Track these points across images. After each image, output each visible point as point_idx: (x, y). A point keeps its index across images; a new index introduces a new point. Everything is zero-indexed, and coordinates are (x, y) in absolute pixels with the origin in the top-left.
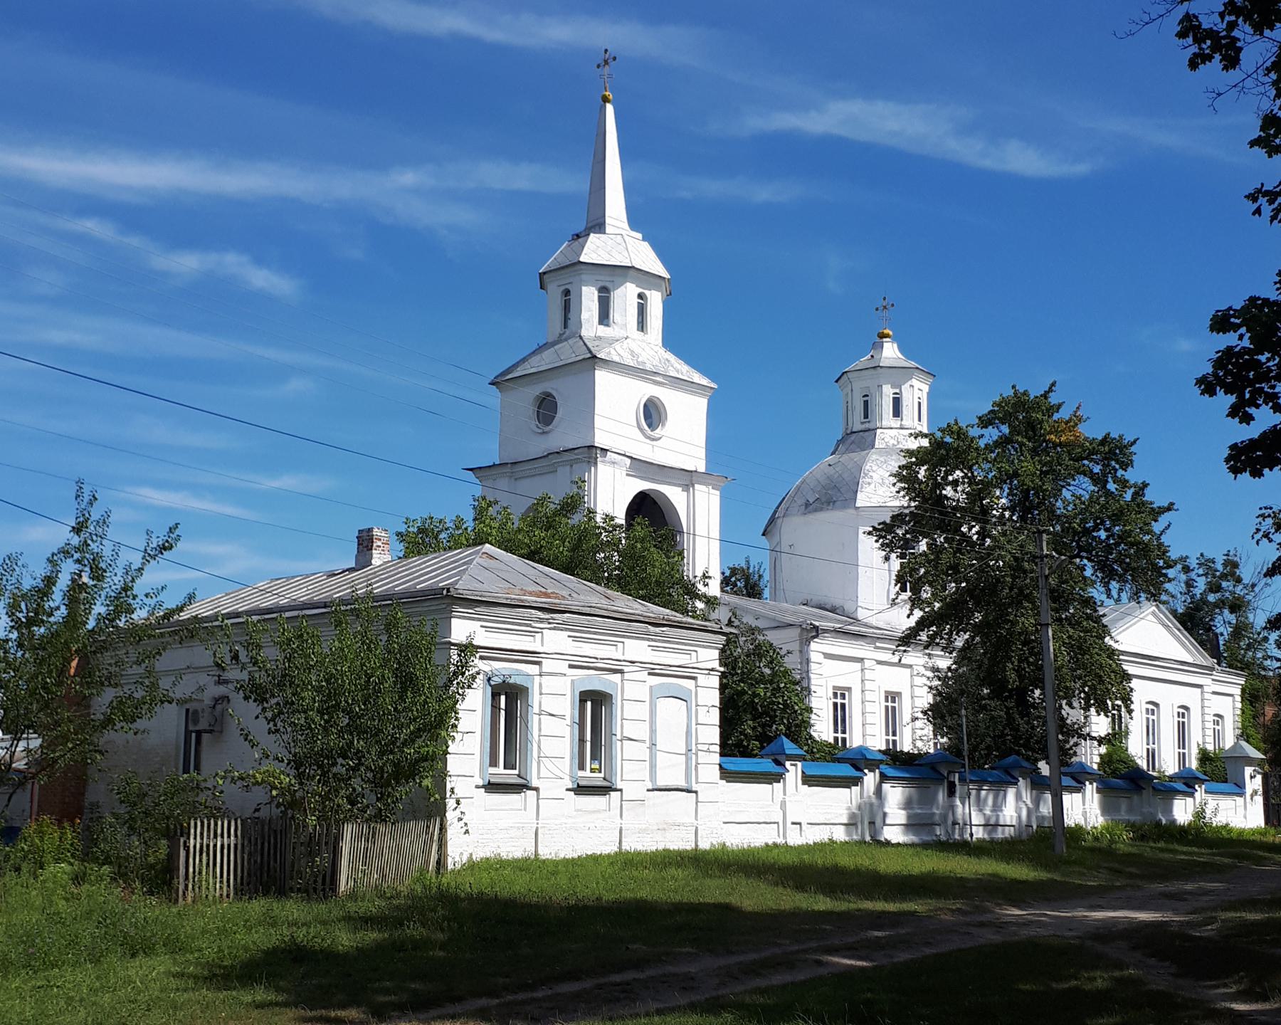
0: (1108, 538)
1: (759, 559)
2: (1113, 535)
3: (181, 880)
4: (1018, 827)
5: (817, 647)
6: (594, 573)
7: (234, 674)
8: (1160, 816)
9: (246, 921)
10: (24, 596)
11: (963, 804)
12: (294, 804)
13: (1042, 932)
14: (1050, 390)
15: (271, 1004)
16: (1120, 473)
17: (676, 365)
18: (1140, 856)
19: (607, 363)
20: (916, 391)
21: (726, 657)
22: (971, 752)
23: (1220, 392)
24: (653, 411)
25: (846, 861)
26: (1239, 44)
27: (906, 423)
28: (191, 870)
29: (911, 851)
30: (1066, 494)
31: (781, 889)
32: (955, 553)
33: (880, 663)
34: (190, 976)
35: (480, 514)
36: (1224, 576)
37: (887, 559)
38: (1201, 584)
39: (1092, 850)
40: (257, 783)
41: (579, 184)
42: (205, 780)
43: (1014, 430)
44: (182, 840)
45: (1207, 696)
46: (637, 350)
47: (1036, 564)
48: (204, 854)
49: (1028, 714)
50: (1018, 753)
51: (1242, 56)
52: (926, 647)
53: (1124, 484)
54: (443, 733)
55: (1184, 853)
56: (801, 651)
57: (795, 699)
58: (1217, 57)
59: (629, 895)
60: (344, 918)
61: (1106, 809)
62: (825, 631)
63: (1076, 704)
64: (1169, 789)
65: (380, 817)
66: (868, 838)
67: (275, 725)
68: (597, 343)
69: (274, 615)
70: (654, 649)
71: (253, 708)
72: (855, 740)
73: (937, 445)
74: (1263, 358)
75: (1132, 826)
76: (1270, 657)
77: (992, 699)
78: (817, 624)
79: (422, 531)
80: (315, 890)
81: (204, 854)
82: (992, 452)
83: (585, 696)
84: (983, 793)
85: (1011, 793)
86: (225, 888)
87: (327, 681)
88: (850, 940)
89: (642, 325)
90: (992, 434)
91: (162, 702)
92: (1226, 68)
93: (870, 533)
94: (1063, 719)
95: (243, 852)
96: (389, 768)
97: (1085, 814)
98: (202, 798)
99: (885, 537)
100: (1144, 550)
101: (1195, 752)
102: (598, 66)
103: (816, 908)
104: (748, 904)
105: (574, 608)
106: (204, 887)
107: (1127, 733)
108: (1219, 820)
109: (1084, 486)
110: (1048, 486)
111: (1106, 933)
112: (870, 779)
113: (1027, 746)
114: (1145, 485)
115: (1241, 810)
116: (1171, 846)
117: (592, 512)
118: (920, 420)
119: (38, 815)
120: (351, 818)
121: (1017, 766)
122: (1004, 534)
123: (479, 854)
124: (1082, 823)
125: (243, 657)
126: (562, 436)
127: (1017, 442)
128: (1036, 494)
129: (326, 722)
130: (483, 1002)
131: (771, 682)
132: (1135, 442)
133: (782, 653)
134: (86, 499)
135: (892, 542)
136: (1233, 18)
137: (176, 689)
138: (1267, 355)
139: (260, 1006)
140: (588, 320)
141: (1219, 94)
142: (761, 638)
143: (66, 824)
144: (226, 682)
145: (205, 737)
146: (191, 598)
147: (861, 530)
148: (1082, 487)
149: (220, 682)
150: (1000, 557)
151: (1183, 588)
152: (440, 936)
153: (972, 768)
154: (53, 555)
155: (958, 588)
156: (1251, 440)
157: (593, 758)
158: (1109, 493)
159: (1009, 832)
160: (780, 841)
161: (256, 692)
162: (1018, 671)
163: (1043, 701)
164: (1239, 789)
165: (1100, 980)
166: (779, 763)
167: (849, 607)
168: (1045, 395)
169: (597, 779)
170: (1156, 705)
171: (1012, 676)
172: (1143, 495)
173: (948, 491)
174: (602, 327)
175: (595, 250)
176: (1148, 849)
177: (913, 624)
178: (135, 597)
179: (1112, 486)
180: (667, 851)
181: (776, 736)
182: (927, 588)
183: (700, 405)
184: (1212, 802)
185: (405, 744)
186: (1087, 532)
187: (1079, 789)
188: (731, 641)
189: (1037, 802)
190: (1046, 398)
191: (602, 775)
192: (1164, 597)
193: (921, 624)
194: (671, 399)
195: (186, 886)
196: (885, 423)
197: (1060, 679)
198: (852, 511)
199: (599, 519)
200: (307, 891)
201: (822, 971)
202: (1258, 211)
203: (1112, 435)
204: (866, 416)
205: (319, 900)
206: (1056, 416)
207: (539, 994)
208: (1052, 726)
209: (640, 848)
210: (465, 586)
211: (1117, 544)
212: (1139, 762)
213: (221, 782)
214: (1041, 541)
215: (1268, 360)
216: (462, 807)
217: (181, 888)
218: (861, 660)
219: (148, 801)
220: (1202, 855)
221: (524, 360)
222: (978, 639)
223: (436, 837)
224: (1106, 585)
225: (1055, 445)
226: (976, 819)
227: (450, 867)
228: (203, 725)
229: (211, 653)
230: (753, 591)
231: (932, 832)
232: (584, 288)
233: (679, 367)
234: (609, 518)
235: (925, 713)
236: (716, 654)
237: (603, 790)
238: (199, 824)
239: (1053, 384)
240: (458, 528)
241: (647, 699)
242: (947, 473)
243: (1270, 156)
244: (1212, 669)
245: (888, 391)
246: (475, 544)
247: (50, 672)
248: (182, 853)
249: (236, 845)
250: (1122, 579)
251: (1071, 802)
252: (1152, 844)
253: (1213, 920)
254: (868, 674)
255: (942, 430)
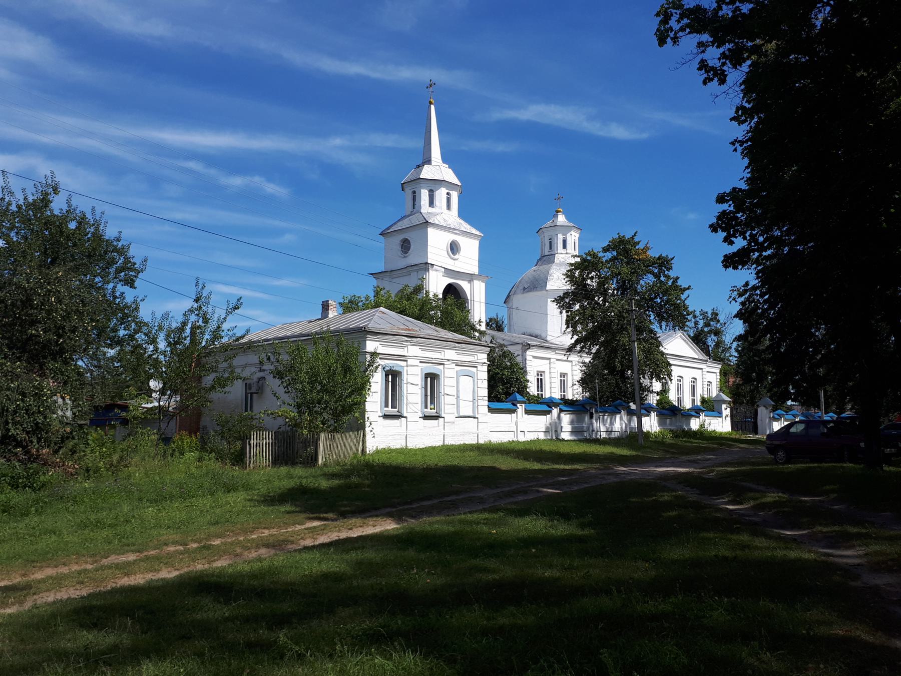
0: (661, 302)
1: (502, 313)
2: (663, 301)
3: (248, 458)
4: (621, 432)
5: (530, 353)
6: (430, 320)
7: (268, 367)
8: (685, 427)
9: (279, 476)
10: (172, 331)
11: (597, 422)
12: (297, 425)
13: (633, 477)
14: (635, 235)
15: (293, 512)
16: (666, 272)
17: (464, 225)
18: (676, 444)
19: (433, 225)
20: (573, 237)
21: (490, 357)
22: (600, 399)
23: (720, 231)
24: (455, 248)
25: (546, 448)
26: (726, 73)
27: (569, 251)
28: (252, 454)
29: (574, 443)
30: (642, 282)
31: (517, 460)
32: (592, 309)
33: (557, 360)
34: (255, 500)
35: (377, 294)
36: (712, 320)
37: (561, 313)
38: (701, 323)
39: (655, 442)
40: (279, 416)
41: (420, 144)
42: (255, 415)
43: (618, 254)
44: (248, 441)
45: (704, 373)
46: (447, 219)
47: (629, 314)
48: (258, 447)
49: (625, 382)
50: (621, 399)
51: (727, 78)
52: (579, 352)
53: (668, 277)
54: (364, 392)
55: (696, 443)
56: (522, 355)
57: (521, 376)
58: (716, 79)
59: (449, 463)
60: (323, 475)
61: (661, 423)
62: (534, 346)
63: (646, 377)
64: (688, 415)
65: (336, 430)
66: (554, 438)
67: (288, 389)
68: (428, 216)
69: (286, 340)
70: (458, 354)
71: (278, 382)
72: (547, 395)
73: (584, 260)
74: (739, 215)
75: (671, 431)
76: (732, 356)
77: (609, 375)
78: (529, 343)
79: (350, 302)
80: (308, 463)
81: (258, 447)
82: (609, 263)
83: (427, 375)
84: (606, 417)
85: (618, 417)
86: (268, 462)
87: (311, 369)
88: (551, 481)
89: (449, 207)
90: (608, 255)
91: (237, 379)
92: (720, 84)
93: (553, 301)
94: (641, 384)
95: (275, 446)
96: (339, 408)
97: (651, 426)
98: (254, 423)
99: (560, 303)
100: (677, 307)
101: (699, 398)
102: (427, 88)
103: (534, 468)
104: (504, 467)
105: (422, 336)
106: (258, 462)
107: (669, 390)
108: (711, 428)
109: (650, 279)
110: (634, 279)
111: (665, 477)
112: (555, 411)
113: (625, 396)
114: (678, 278)
115: (720, 424)
116: (689, 440)
117: (427, 292)
118: (575, 250)
119: (179, 431)
120: (323, 430)
121: (621, 405)
122: (614, 301)
123: (381, 447)
124: (650, 430)
125: (272, 358)
126: (413, 258)
127: (620, 259)
128: (628, 283)
129: (312, 387)
130: (388, 510)
131: (510, 369)
132: (673, 258)
133: (515, 355)
134: (200, 287)
135: (563, 305)
136: (724, 60)
137: (243, 372)
138: (741, 214)
139: (288, 513)
140: (424, 205)
141: (717, 96)
142: (505, 349)
143: (193, 435)
144: (264, 371)
145: (255, 395)
146: (248, 331)
147: (549, 300)
148: (650, 279)
149: (261, 371)
150: (613, 311)
151: (693, 325)
152: (367, 482)
153: (600, 406)
154: (186, 312)
155: (593, 326)
156: (733, 253)
157: (431, 403)
158: (661, 282)
159: (617, 434)
160: (515, 439)
161: (279, 375)
162: (621, 362)
163: (632, 376)
164: (720, 414)
165: (666, 497)
166: (514, 405)
167: (543, 335)
168: (633, 238)
169: (433, 412)
170: (682, 377)
171: (618, 365)
172: (677, 282)
173: (589, 281)
174: (430, 208)
175: (427, 172)
176: (680, 441)
177: (573, 342)
178: (223, 331)
179: (663, 279)
180: (465, 444)
181: (512, 393)
182: (579, 325)
183: (475, 244)
184: (708, 420)
185: (346, 397)
186: (652, 299)
187: (648, 415)
188: (492, 350)
189: (630, 421)
190: (633, 239)
191: (435, 411)
192: (686, 328)
193: (577, 342)
194: (462, 241)
195: (250, 462)
196: (559, 252)
197: (640, 366)
198: (544, 292)
199: (431, 296)
200: (304, 463)
201: (541, 495)
202: (735, 150)
203: (663, 256)
204: (551, 248)
205: (310, 467)
206: (637, 247)
207: (414, 506)
208: (637, 387)
209: (453, 443)
210: (372, 326)
211: (665, 305)
212: (674, 403)
213: (262, 416)
214: (632, 303)
215: (742, 216)
216: (372, 426)
217: (248, 462)
218: (549, 359)
219: (230, 424)
220: (704, 444)
221: (395, 224)
222: (602, 348)
223: (361, 439)
224: (660, 323)
225: (637, 260)
226: (603, 429)
227: (368, 452)
228: (254, 390)
229: (258, 357)
230: (499, 328)
231: (583, 435)
232: (422, 190)
233: (466, 226)
234: (436, 295)
235: (578, 382)
236: (486, 356)
237: (436, 417)
238: (255, 433)
239: (636, 232)
240: (367, 300)
241: (455, 376)
242: (588, 274)
243: (739, 125)
244: (707, 361)
245: (560, 237)
246: (375, 308)
247: (185, 365)
248: (248, 447)
249: (272, 443)
250: (667, 321)
251: (645, 420)
252: (681, 439)
253: (712, 471)
254: (553, 365)
255: (586, 254)
